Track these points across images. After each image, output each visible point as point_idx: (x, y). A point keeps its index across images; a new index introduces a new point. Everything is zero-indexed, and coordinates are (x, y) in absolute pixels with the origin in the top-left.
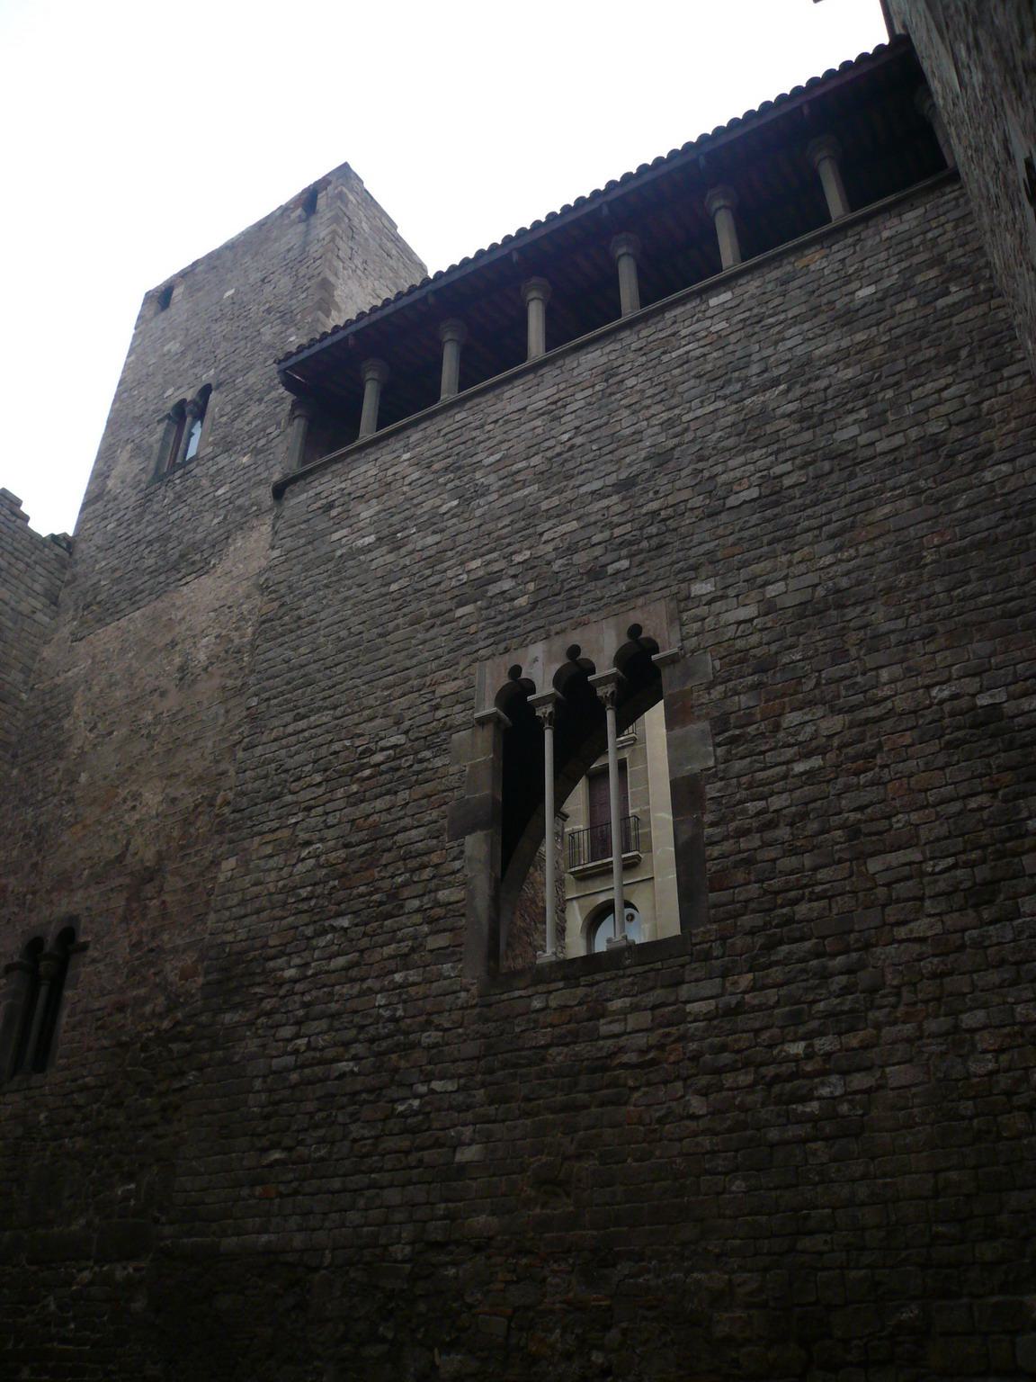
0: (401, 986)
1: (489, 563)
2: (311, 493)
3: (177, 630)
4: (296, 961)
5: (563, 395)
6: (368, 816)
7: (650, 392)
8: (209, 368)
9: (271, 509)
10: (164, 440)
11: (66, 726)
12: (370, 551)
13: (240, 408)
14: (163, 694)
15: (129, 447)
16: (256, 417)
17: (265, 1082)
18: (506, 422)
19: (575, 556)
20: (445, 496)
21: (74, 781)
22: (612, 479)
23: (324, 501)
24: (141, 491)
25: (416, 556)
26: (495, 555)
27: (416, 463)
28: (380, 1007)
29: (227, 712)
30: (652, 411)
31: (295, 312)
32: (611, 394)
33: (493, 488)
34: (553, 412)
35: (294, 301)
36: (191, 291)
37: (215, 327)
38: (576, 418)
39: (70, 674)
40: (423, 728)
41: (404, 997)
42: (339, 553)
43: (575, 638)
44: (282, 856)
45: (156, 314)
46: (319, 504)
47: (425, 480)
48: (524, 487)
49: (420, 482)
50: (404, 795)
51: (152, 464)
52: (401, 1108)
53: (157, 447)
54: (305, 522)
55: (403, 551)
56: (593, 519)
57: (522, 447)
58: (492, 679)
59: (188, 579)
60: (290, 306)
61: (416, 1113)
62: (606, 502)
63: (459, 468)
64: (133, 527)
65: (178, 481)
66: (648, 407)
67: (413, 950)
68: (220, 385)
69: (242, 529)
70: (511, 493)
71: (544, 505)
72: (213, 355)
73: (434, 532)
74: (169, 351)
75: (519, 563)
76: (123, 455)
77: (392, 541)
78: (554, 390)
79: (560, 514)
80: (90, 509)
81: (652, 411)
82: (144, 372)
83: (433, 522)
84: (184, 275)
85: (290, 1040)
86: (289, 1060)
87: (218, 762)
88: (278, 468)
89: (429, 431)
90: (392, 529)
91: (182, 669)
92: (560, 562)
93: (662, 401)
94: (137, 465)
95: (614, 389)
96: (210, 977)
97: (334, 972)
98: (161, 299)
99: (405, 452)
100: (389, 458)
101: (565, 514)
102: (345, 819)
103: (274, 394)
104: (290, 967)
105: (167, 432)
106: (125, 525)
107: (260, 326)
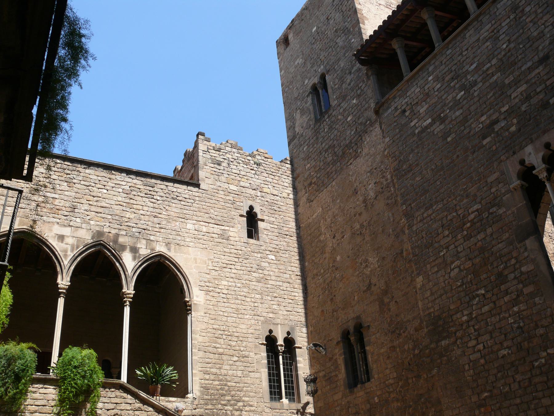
0: (518, 313)
1: (490, 115)
2: (393, 108)
3: (355, 185)
4: (466, 312)
5: (495, 26)
6: (476, 244)
7: (539, 11)
8: (320, 66)
9: (376, 121)
10: (313, 103)
11: (322, 239)
12: (432, 126)
13: (342, 80)
14: (360, 214)
15: (298, 111)
16: (351, 81)
17: (469, 366)
18: (472, 48)
19: (532, 100)
20: (457, 91)
21: (335, 261)
22: (536, 59)
23: (400, 110)
24: (312, 129)
25: (454, 122)
26: (492, 111)
27: (436, 79)
28: (511, 323)
29: (393, 214)
30: (545, 19)
31: (349, 28)
32: (520, 18)
33: (479, 80)
34: (494, 37)
35: (346, 23)
36: (297, 34)
37: (314, 46)
38: (506, 35)
39: (314, 216)
40: (487, 199)
41: (521, 316)
42: (417, 131)
43: (546, 138)
44: (443, 271)
45: (285, 49)
46: (399, 112)
47: (444, 87)
48: (493, 75)
49: (442, 88)
50: (489, 231)
51: (313, 116)
52: (536, 364)
53: (311, 108)
54: (395, 122)
55: (447, 122)
56: (533, 81)
57: (485, 57)
58: (512, 168)
59: (351, 161)
60: (345, 26)
61: (544, 365)
62: (537, 71)
63: (458, 76)
64: (315, 146)
65: (327, 120)
66: (541, 18)
67: (518, 296)
68: (328, 71)
69: (366, 133)
70: (488, 80)
71: (507, 81)
72: (319, 59)
73: (458, 109)
74: (298, 63)
75: (505, 112)
76: (298, 116)
77: (439, 119)
78: (490, 25)
79: (516, 83)
80: (293, 143)
81: (545, 19)
82: (291, 76)
83: (457, 104)
84: (290, 28)
85: (474, 347)
86: (478, 355)
87: (398, 237)
88: (372, 101)
89: (436, 64)
90: (438, 113)
91: (365, 201)
92: (524, 106)
93: (548, 12)
94: (305, 118)
95: (520, 15)
96: (429, 328)
97: (485, 313)
98: (284, 42)
99: (429, 77)
100: (422, 82)
101: (519, 82)
102: (466, 247)
103: (355, 68)
104: (464, 316)
105: (312, 99)
106: (311, 146)
107: (335, 39)
